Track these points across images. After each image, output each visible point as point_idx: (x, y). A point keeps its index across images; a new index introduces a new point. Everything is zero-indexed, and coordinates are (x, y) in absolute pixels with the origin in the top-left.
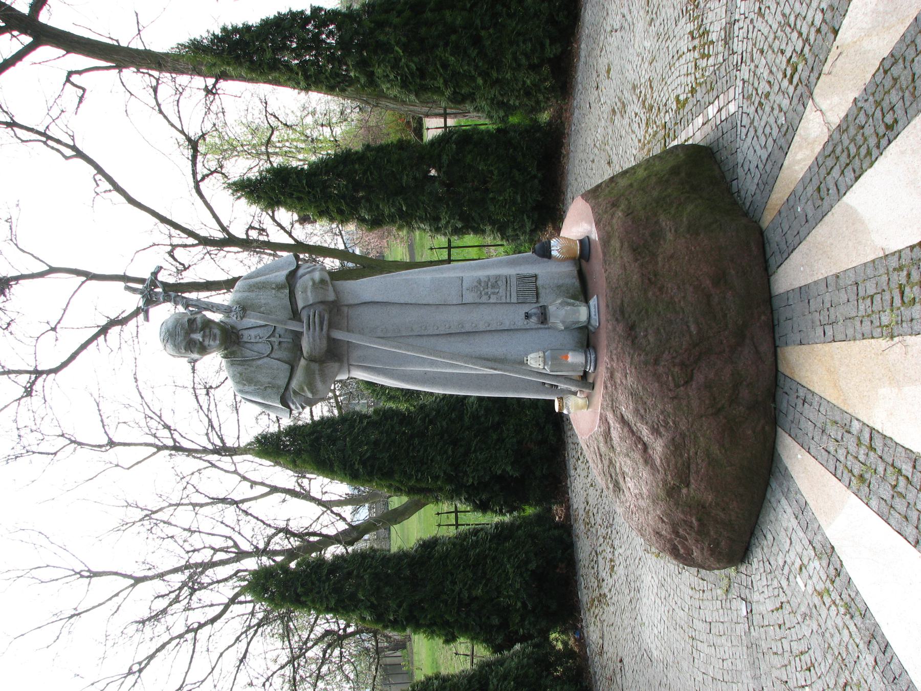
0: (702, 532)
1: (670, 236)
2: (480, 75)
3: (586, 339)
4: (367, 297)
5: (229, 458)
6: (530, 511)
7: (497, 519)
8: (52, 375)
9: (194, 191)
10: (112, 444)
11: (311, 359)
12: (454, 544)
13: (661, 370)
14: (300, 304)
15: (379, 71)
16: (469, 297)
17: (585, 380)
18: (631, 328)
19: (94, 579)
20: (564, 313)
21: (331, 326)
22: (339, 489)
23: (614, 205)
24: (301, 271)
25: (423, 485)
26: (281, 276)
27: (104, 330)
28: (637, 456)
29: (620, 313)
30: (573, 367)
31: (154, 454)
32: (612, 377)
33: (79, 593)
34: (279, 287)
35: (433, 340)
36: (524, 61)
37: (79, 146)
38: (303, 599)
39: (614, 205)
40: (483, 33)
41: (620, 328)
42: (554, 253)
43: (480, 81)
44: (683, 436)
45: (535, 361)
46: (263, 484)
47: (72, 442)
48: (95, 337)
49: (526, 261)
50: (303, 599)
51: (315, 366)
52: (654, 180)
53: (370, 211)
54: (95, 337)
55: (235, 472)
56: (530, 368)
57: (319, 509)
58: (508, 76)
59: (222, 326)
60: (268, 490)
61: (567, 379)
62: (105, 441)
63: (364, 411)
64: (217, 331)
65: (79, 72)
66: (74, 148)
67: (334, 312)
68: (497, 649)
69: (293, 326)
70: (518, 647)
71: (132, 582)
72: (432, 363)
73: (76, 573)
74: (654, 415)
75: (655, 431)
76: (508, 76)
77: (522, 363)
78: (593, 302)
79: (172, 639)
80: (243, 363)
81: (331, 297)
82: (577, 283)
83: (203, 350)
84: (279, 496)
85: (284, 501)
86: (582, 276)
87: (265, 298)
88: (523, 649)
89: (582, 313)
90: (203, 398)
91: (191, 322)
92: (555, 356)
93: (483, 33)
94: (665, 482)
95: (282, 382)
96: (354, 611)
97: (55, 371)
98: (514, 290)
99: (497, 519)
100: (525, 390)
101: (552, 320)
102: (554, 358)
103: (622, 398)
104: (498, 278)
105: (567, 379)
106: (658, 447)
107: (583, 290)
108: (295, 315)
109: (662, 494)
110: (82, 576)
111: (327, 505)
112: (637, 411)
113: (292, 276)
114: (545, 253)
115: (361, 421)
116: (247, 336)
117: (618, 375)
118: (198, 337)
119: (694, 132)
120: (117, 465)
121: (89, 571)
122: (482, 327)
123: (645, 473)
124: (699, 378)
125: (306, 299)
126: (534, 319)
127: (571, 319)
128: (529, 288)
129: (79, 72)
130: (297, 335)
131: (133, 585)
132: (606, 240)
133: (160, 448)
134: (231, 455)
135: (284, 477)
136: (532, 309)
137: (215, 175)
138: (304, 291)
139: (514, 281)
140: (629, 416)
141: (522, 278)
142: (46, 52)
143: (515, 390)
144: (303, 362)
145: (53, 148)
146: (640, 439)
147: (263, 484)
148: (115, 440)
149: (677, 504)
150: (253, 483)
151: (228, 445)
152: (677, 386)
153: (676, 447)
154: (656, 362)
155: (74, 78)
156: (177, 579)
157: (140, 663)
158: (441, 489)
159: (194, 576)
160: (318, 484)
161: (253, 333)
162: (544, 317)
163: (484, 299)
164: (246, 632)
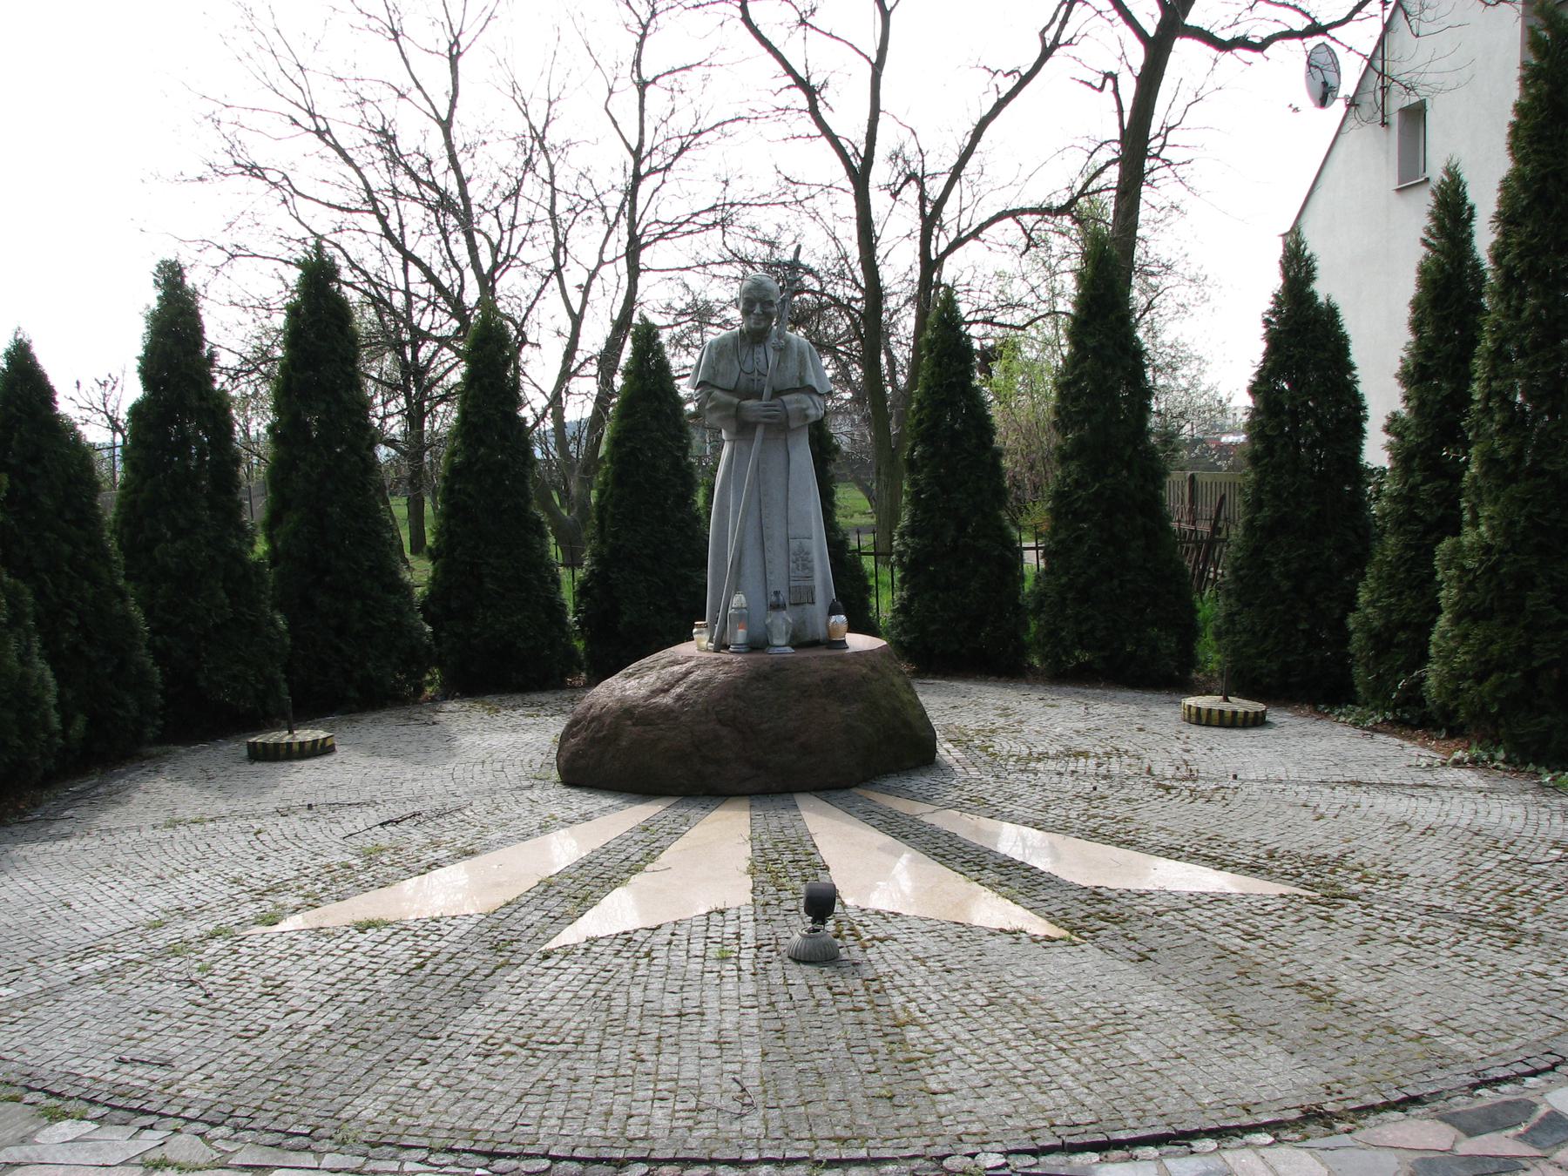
0: (593, 742)
1: (844, 710)
2: (1379, 676)
3: (757, 645)
4: (794, 456)
5: (623, 251)
6: (580, 645)
7: (570, 605)
8: (739, 14)
9: (1000, 209)
10: (642, 86)
11: (738, 408)
12: (542, 556)
13: (730, 700)
14: (786, 398)
15: (1073, 466)
16: (794, 544)
17: (721, 646)
18: (766, 677)
19: (447, 62)
20: (781, 625)
21: (767, 426)
22: (578, 410)
23: (873, 668)
24: (815, 398)
25: (608, 523)
26: (812, 380)
27: (803, 84)
28: (658, 684)
29: (778, 668)
30: (734, 634)
31: (628, 146)
32: (725, 663)
33: (426, 35)
34: (801, 379)
35: (756, 514)
36: (1084, 628)
37: (1057, 52)
38: (476, 385)
39: (873, 668)
40: (1116, 582)
41: (767, 668)
42: (833, 618)
43: (1064, 580)
44: (676, 718)
45: (738, 600)
46: (585, 302)
47: (645, 27)
48: (790, 70)
49: (827, 594)
50: (476, 385)
51: (732, 411)
52: (898, 705)
53: (921, 456)
54: (790, 70)
55: (601, 263)
56: (731, 597)
57: (549, 388)
58: (1069, 611)
59: (767, 330)
60: (577, 310)
61: (723, 630)
62: (647, 75)
63: (694, 451)
64: (763, 325)
65: (1116, 91)
66: (1056, 44)
67: (780, 427)
68: (424, 608)
69: (767, 392)
70: (428, 629)
71: (444, 117)
72: (736, 512)
73: (456, 38)
74: (692, 695)
75: (679, 697)
76: (1069, 611)
77: (737, 590)
78: (789, 649)
79: (358, 170)
80: (735, 345)
81: (793, 425)
82: (808, 639)
83: (746, 313)
84: (566, 325)
85: (559, 333)
86: (815, 644)
87: (792, 366)
88: (426, 634)
89: (780, 640)
90: (709, 218)
91: (771, 303)
92: (743, 617)
93: (1116, 582)
94: (636, 707)
95: (719, 382)
96: (464, 443)
97: (746, 19)
98: (802, 583)
99: (570, 605)
100: (714, 595)
101: (774, 614)
102: (741, 616)
103: (707, 671)
104: (812, 569)
105: (723, 630)
106: (666, 700)
107: (799, 641)
108: (777, 393)
109: (627, 705)
110: (451, 46)
111: (556, 402)
112: (696, 682)
113: (812, 390)
114: (833, 611)
115: (680, 448)
116: (759, 350)
117: (727, 668)
118: (757, 309)
119: (946, 751)
120: (611, 91)
121: (459, 54)
122: (768, 555)
123: (643, 692)
124: (724, 731)
125: (790, 402)
126: (774, 599)
127: (775, 631)
128: (803, 597)
129: (1116, 91)
130: (759, 396)
131: (439, 120)
132: (842, 659)
133: (637, 154)
134: (627, 254)
135: (594, 336)
136: (784, 596)
137: (1025, 240)
138: (798, 401)
139: (807, 584)
140: (692, 677)
141: (811, 591)
142: (1137, 55)
143: (713, 587)
144: (736, 401)
145: (1055, 16)
146: (672, 686)
147: (585, 302)
148: (649, 90)
149: (618, 717)
150: (585, 290)
151: (643, 253)
152: (717, 713)
153: (666, 713)
154: (737, 697)
155: (1109, 83)
156: (450, 184)
157: (328, 131)
158: (603, 542)
159: (454, 209)
160: (585, 387)
161: (762, 356)
162: (776, 607)
163: (792, 557)
164: (369, 280)
